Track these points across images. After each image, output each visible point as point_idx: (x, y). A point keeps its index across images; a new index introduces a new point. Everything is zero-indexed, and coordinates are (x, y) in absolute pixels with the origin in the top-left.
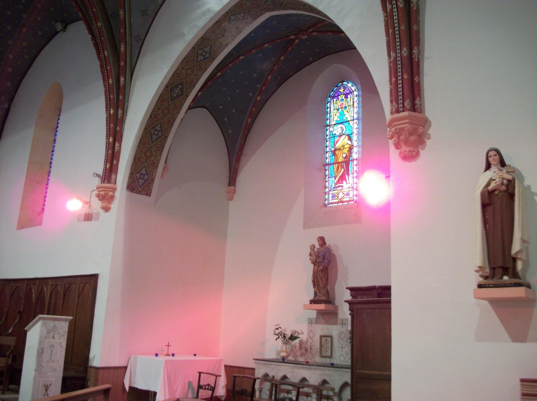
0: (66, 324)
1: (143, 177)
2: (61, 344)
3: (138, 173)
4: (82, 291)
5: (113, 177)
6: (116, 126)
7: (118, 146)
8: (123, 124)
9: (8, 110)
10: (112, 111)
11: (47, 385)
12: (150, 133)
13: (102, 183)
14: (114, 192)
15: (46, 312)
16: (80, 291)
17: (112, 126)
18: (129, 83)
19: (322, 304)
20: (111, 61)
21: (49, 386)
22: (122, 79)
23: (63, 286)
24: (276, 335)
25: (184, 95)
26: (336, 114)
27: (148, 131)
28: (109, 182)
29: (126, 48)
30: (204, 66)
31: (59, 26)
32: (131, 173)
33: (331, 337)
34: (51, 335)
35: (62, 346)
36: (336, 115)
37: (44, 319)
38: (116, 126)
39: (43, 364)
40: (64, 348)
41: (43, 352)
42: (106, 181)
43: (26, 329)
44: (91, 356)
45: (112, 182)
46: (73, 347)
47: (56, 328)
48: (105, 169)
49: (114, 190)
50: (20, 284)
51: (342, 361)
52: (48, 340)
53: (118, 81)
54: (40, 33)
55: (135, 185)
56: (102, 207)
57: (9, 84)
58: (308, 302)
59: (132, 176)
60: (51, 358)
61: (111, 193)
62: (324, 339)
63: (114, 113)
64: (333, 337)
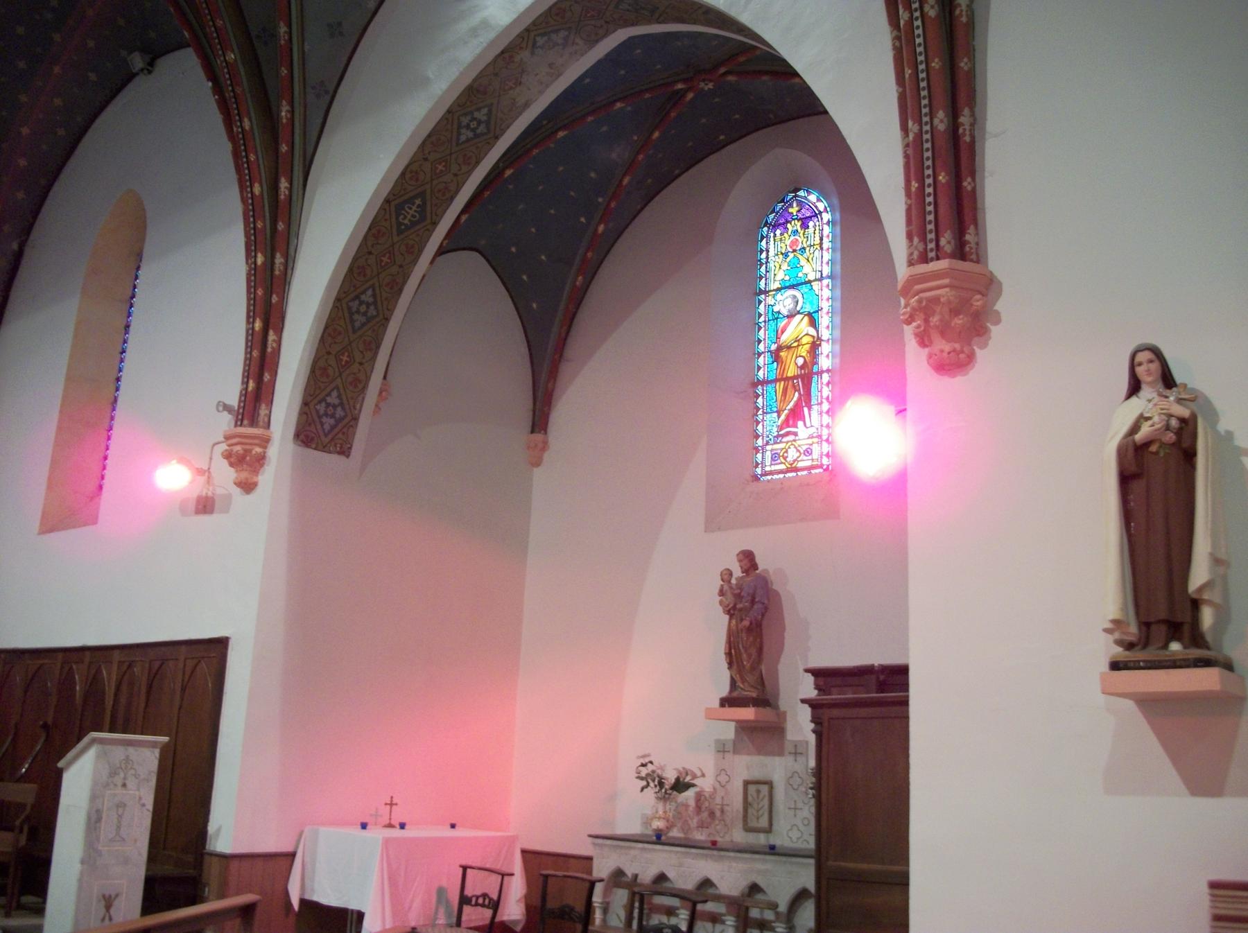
0: (154, 753)
1: (332, 411)
2: (143, 801)
3: (320, 402)
4: (190, 677)
5: (263, 411)
6: (269, 293)
7: (274, 341)
8: (287, 287)
9: (18, 257)
10: (260, 259)
11: (110, 896)
12: (349, 308)
13: (236, 425)
14: (265, 447)
16: (187, 677)
17: (260, 294)
18: (301, 192)
19: (749, 706)
20: (258, 141)
21: (115, 899)
22: (284, 184)
23: (147, 665)
24: (642, 779)
25: (429, 221)
26: (780, 266)
27: (344, 305)
28: (253, 423)
29: (292, 112)
30: (474, 153)
31: (137, 61)
32: (305, 404)
33: (770, 784)
34: (118, 780)
35: (143, 805)
36: (780, 268)
37: (101, 741)
38: (269, 293)
39: (100, 848)
40: (148, 810)
41: (99, 820)
42: (246, 422)
43: (60, 764)
44: (211, 828)
45: (261, 423)
46: (169, 807)
47: (131, 762)
48: (244, 394)
49: (265, 442)
50: (46, 661)
51: (794, 839)
52: (113, 792)
53: (274, 188)
54: (93, 76)
55: (314, 430)
56: (237, 481)
57: (20, 195)
58: (717, 704)
59: (306, 409)
60: (118, 833)
61: (258, 450)
62: (752, 788)
63: (264, 264)
64: (775, 784)
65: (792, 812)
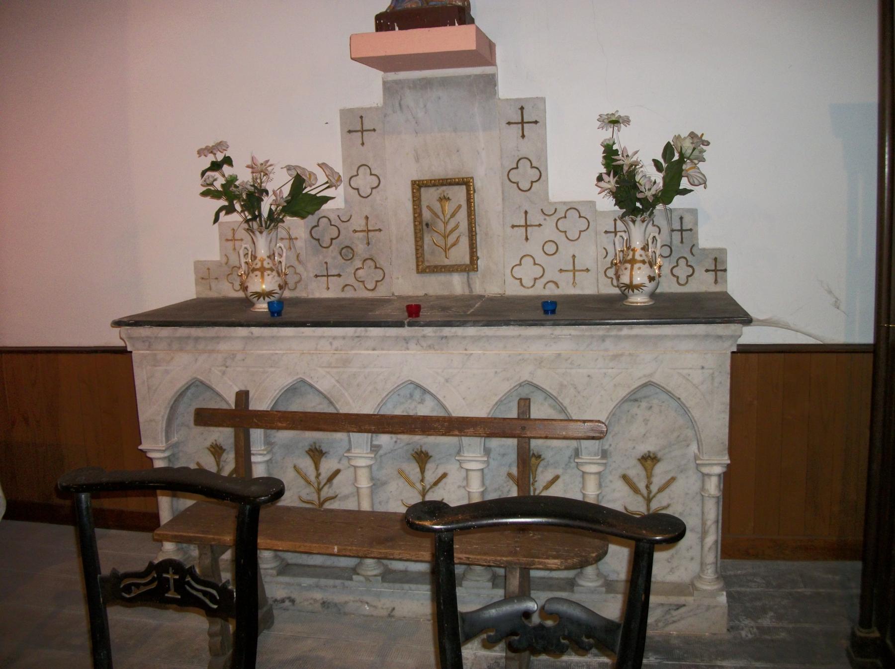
5: (145, 451)
15: (487, 70)
19: (453, 24)
24: (216, 195)
33: (466, 183)
51: (528, 282)
58: (370, 26)
62: (429, 196)
64: (478, 184)
65: (711, 275)
